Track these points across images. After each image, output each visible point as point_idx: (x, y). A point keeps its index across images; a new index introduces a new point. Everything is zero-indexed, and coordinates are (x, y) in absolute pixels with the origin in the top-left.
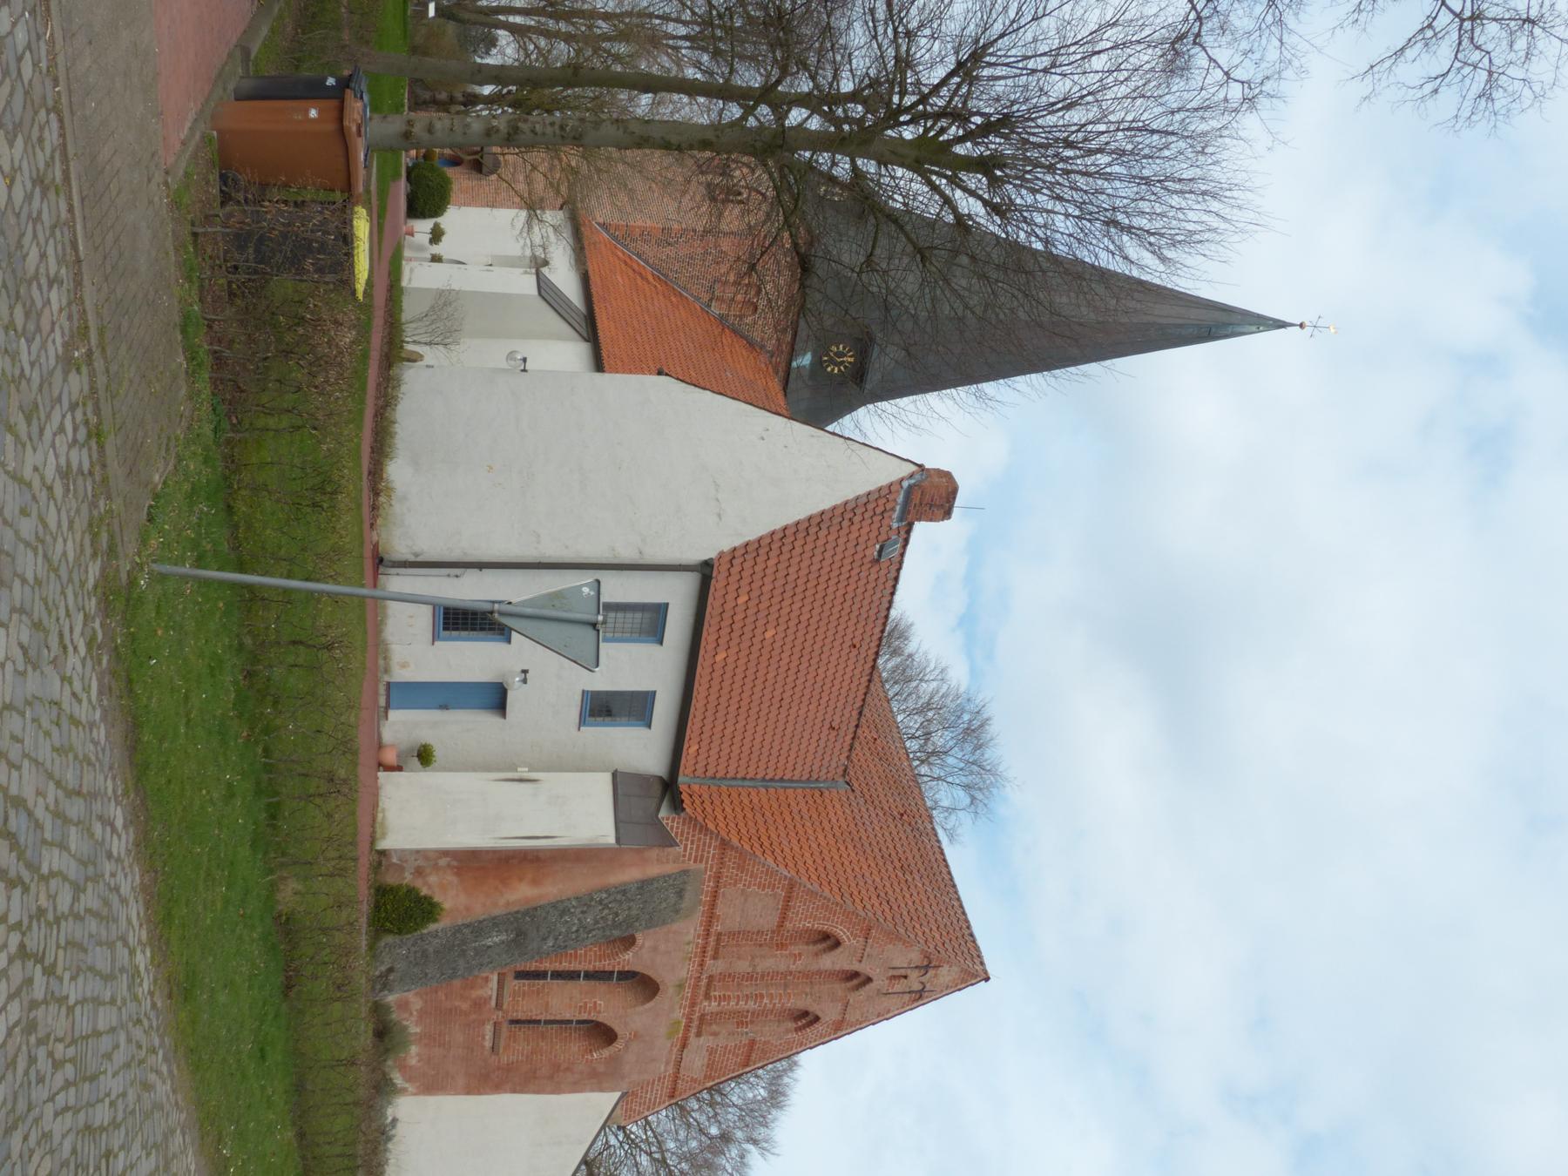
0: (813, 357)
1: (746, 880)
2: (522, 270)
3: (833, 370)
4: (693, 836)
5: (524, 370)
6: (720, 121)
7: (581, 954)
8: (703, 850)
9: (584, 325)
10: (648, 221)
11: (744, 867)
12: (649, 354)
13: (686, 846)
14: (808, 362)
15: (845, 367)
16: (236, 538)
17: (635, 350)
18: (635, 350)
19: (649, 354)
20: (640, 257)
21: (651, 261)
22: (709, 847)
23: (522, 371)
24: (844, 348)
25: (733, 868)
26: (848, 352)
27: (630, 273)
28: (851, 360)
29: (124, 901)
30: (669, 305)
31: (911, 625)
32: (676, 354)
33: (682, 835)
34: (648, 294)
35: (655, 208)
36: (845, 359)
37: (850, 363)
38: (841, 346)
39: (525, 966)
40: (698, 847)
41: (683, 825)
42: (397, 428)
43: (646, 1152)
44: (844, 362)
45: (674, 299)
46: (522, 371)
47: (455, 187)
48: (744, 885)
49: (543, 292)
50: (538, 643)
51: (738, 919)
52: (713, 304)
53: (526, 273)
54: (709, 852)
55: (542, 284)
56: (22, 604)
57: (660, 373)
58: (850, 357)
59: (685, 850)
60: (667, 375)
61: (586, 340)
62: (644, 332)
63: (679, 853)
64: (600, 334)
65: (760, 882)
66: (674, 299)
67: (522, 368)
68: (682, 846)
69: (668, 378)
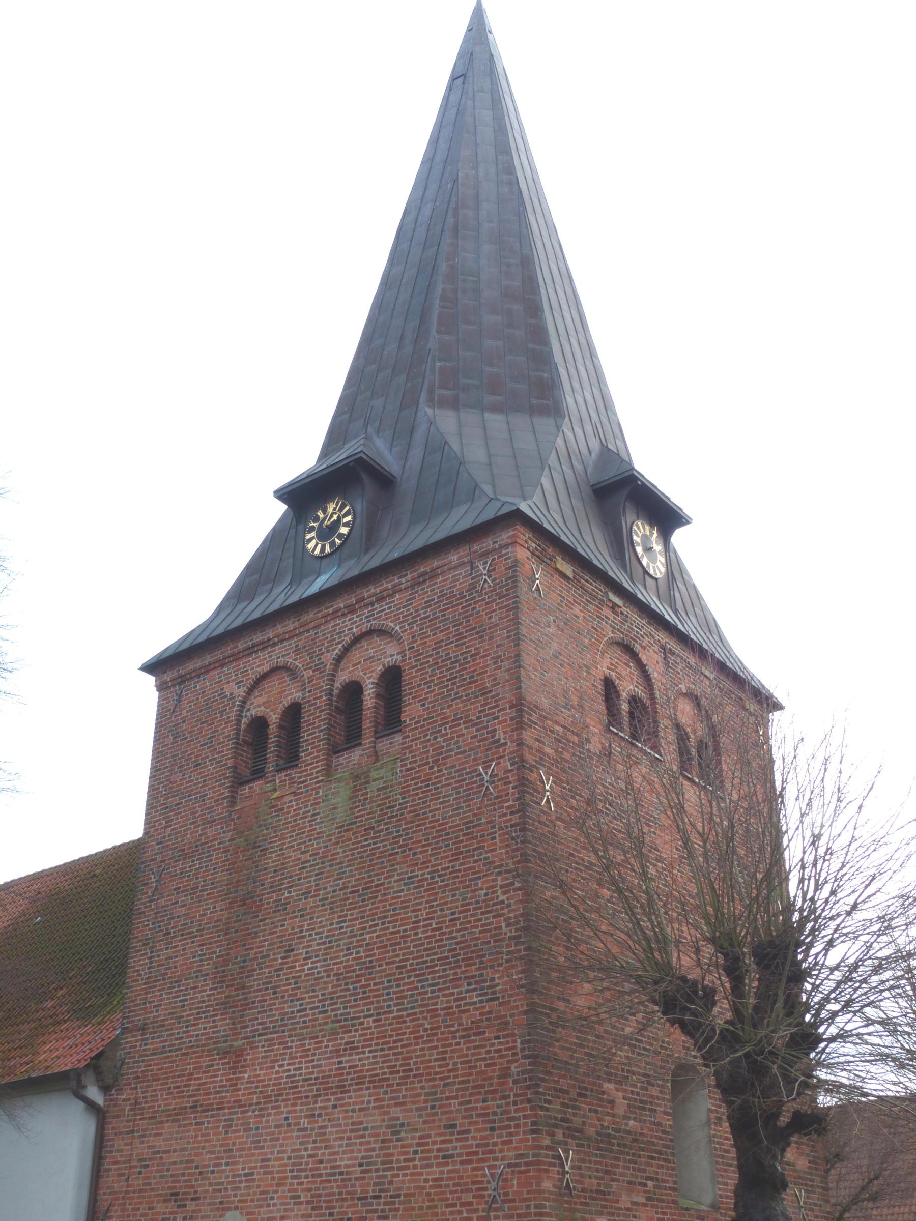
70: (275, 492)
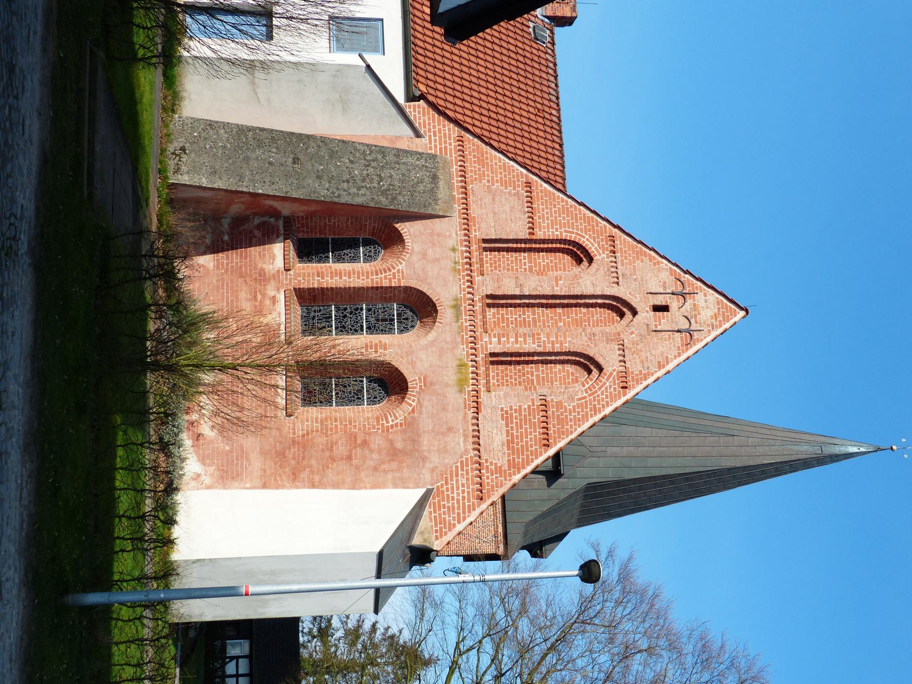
1: (488, 176)
4: (434, 127)
6: (157, 443)
7: (521, 337)
8: (445, 142)
11: (483, 160)
13: (430, 136)
22: (450, 139)
25: (475, 162)
31: (178, 574)
33: (435, 132)
39: (408, 242)
40: (440, 137)
41: (424, 116)
43: (141, 8)
48: (488, 181)
50: (715, 415)
51: (493, 224)
54: (450, 144)
56: (253, 83)
59: (430, 143)
63: (426, 145)
65: (501, 178)
68: (427, 138)
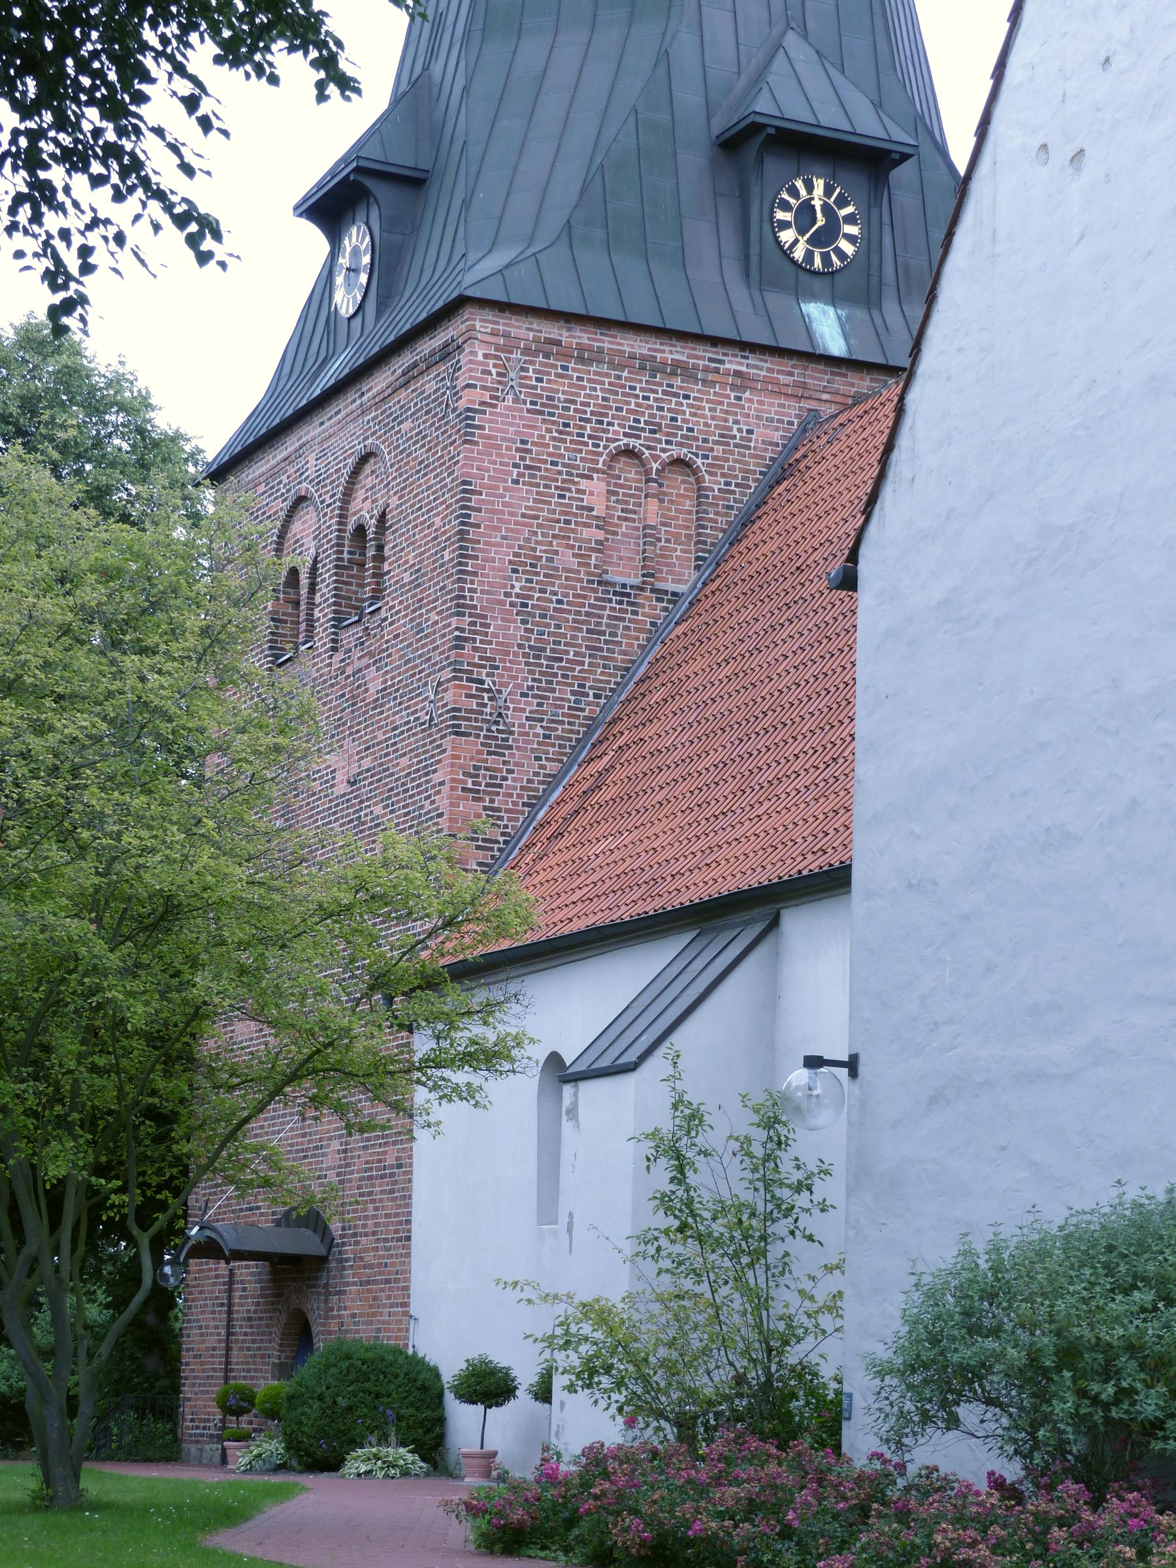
0: (814, 297)
2: (567, 1126)
3: (851, 239)
5: (852, 1065)
9: (728, 935)
10: (436, 778)
12: (815, 741)
14: (830, 310)
15: (842, 202)
16: (453, 1060)
17: (800, 783)
18: (800, 783)
19: (815, 741)
20: (541, 800)
21: (552, 768)
23: (854, 1074)
24: (785, 206)
26: (794, 192)
27: (584, 819)
28: (819, 185)
29: (216, 1269)
30: (674, 706)
32: (814, 669)
34: (643, 766)
35: (404, 761)
36: (817, 203)
37: (828, 191)
38: (780, 215)
42: (1054, 1216)
44: (826, 208)
45: (657, 696)
46: (854, 1074)
47: (363, 1333)
49: (631, 1057)
52: (670, 587)
53: (573, 1113)
55: (605, 1062)
57: (849, 581)
58: (810, 188)
60: (853, 556)
61: (774, 923)
62: (750, 764)
64: (752, 881)
66: (657, 696)
67: (843, 1072)
69: (864, 551)
70: (296, 208)
